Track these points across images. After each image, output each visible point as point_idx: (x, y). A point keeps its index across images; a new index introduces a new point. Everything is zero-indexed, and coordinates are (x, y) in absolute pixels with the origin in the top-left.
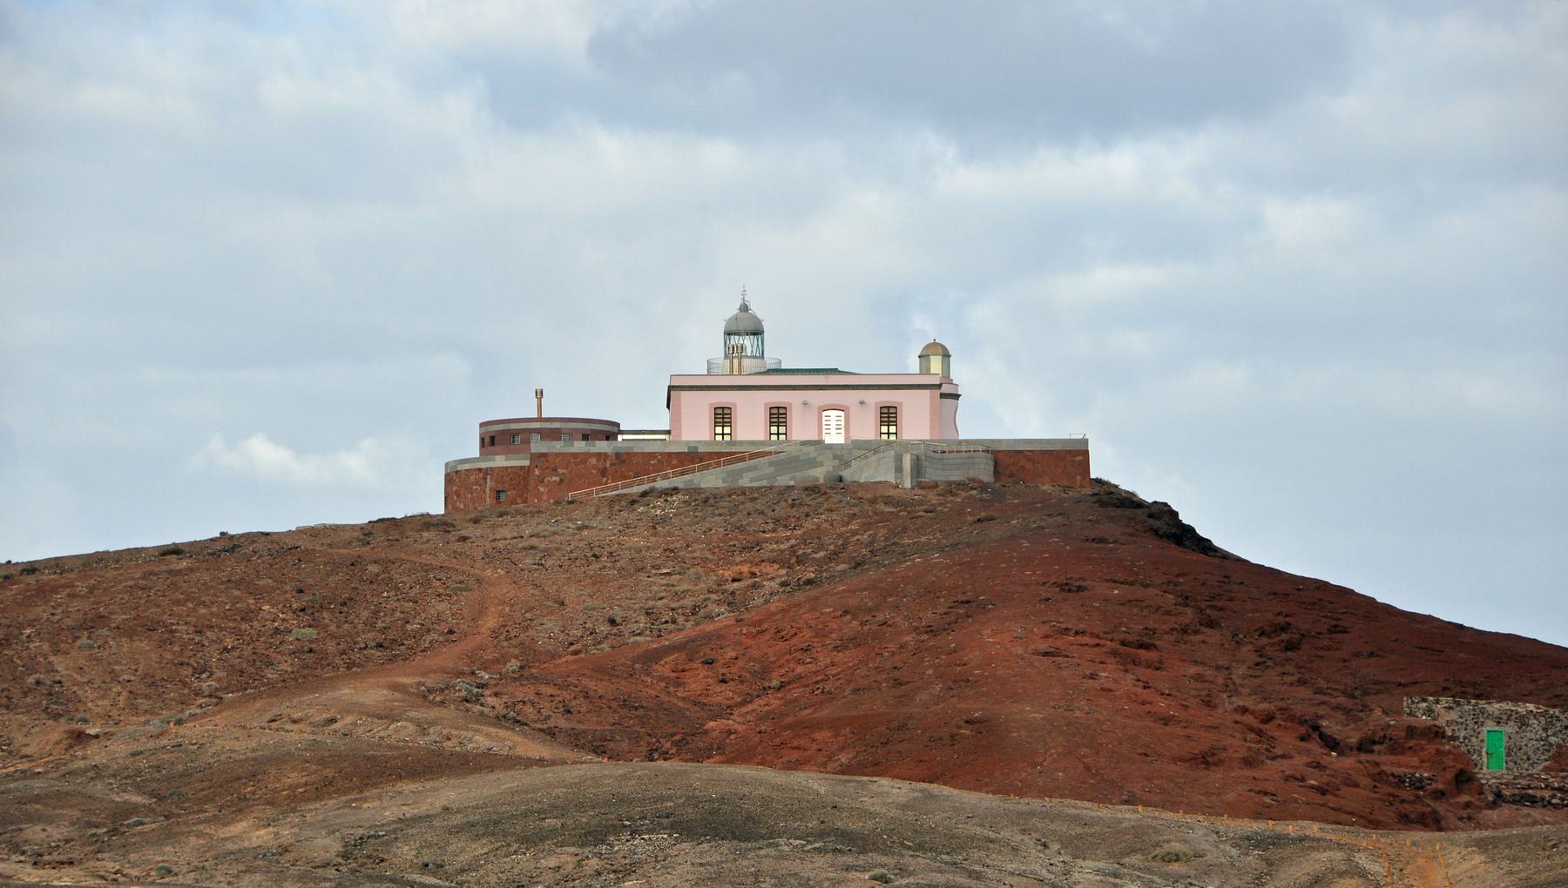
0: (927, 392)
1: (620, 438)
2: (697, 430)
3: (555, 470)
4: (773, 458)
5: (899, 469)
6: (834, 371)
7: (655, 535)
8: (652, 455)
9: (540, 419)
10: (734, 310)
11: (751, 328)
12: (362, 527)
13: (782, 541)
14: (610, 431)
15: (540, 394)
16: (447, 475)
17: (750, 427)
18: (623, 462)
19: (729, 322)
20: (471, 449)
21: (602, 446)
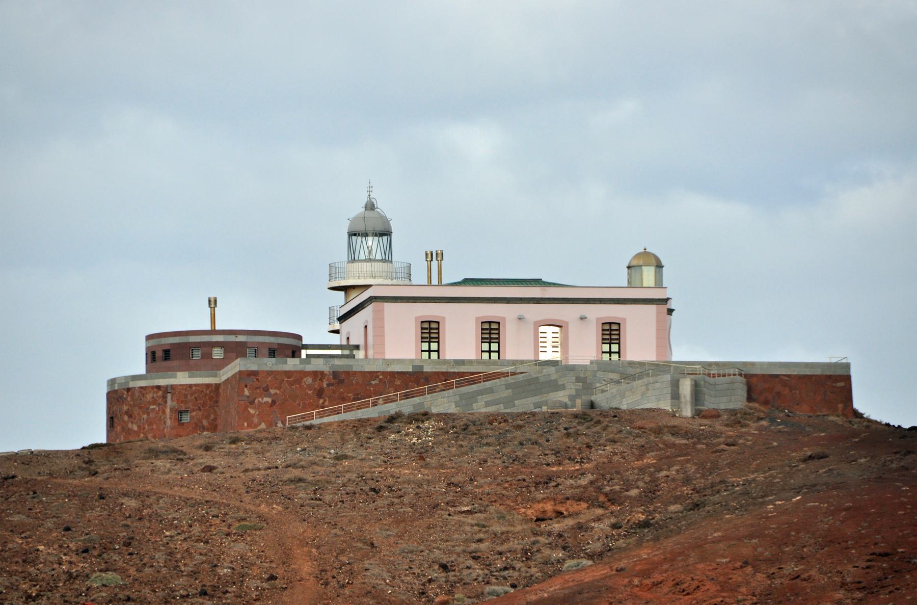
0: (653, 308)
1: (304, 353)
2: (400, 347)
3: (266, 390)
4: (510, 379)
5: (676, 396)
6: (537, 282)
7: (427, 466)
8: (373, 375)
9: (213, 332)
10: (359, 209)
11: (380, 228)
12: (77, 454)
13: (577, 477)
14: (290, 346)
15: (213, 303)
16: (108, 394)
17: (461, 345)
18: (341, 382)
19: (353, 221)
20: (134, 364)
21: (292, 364)
